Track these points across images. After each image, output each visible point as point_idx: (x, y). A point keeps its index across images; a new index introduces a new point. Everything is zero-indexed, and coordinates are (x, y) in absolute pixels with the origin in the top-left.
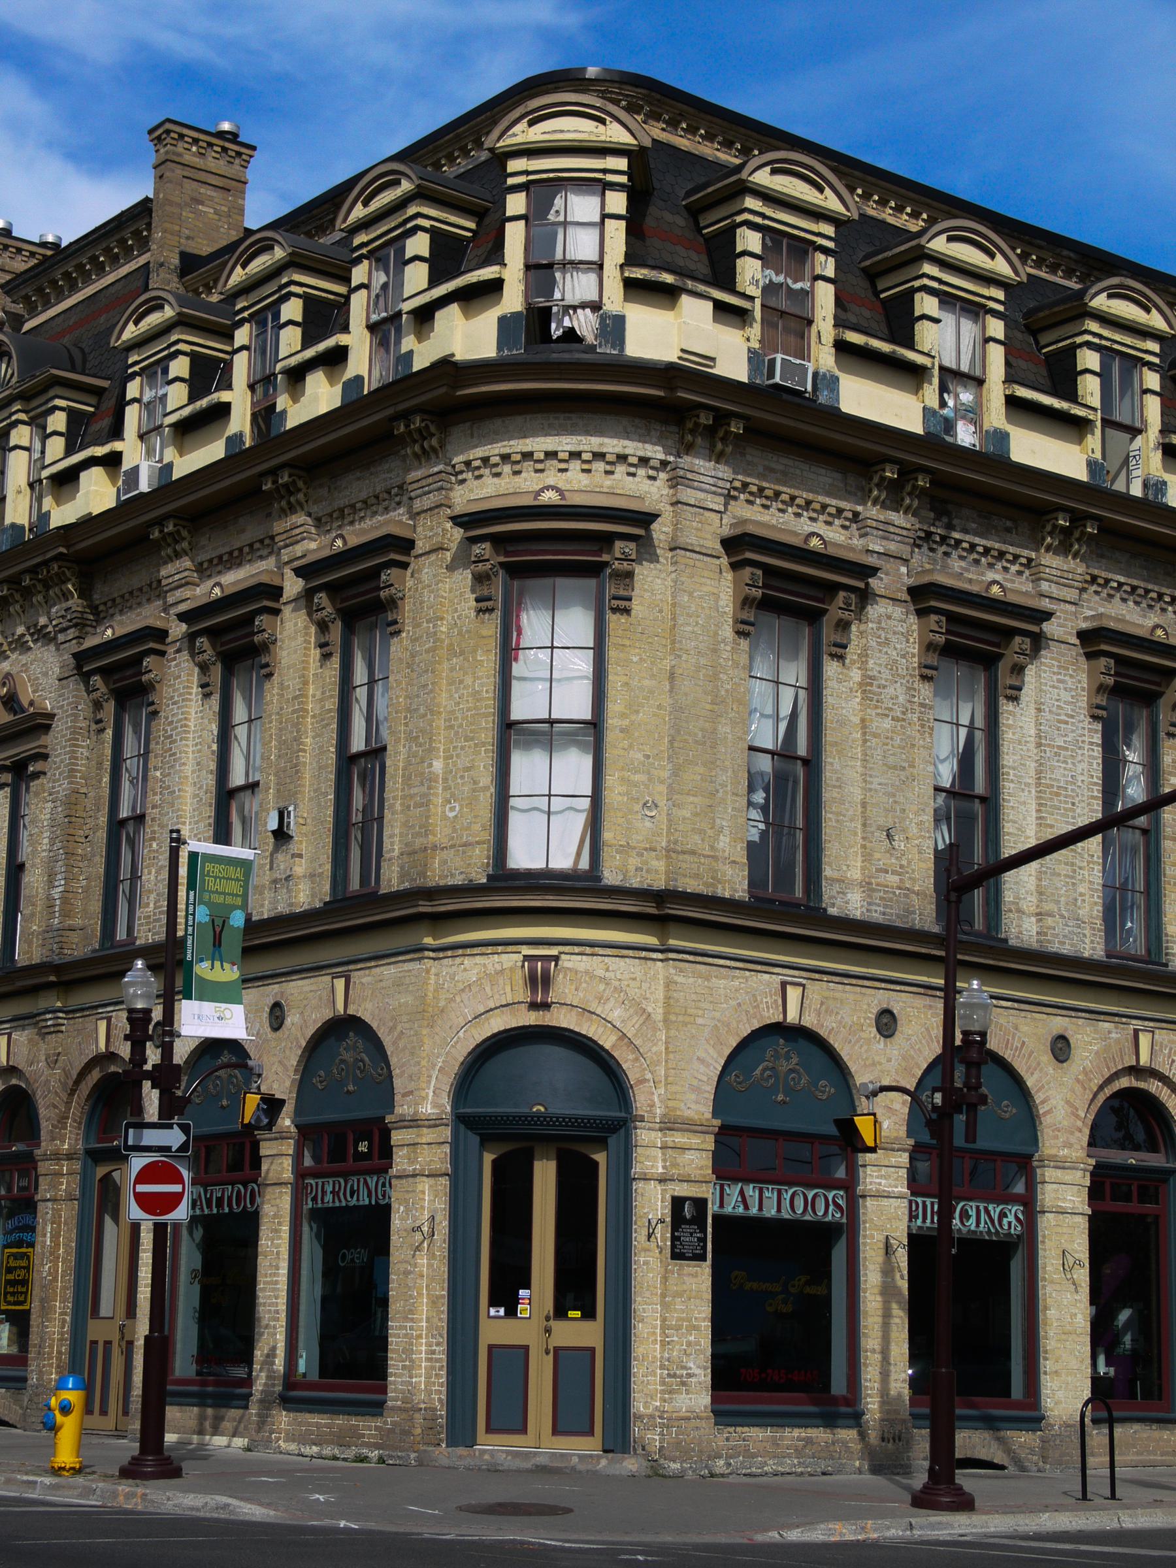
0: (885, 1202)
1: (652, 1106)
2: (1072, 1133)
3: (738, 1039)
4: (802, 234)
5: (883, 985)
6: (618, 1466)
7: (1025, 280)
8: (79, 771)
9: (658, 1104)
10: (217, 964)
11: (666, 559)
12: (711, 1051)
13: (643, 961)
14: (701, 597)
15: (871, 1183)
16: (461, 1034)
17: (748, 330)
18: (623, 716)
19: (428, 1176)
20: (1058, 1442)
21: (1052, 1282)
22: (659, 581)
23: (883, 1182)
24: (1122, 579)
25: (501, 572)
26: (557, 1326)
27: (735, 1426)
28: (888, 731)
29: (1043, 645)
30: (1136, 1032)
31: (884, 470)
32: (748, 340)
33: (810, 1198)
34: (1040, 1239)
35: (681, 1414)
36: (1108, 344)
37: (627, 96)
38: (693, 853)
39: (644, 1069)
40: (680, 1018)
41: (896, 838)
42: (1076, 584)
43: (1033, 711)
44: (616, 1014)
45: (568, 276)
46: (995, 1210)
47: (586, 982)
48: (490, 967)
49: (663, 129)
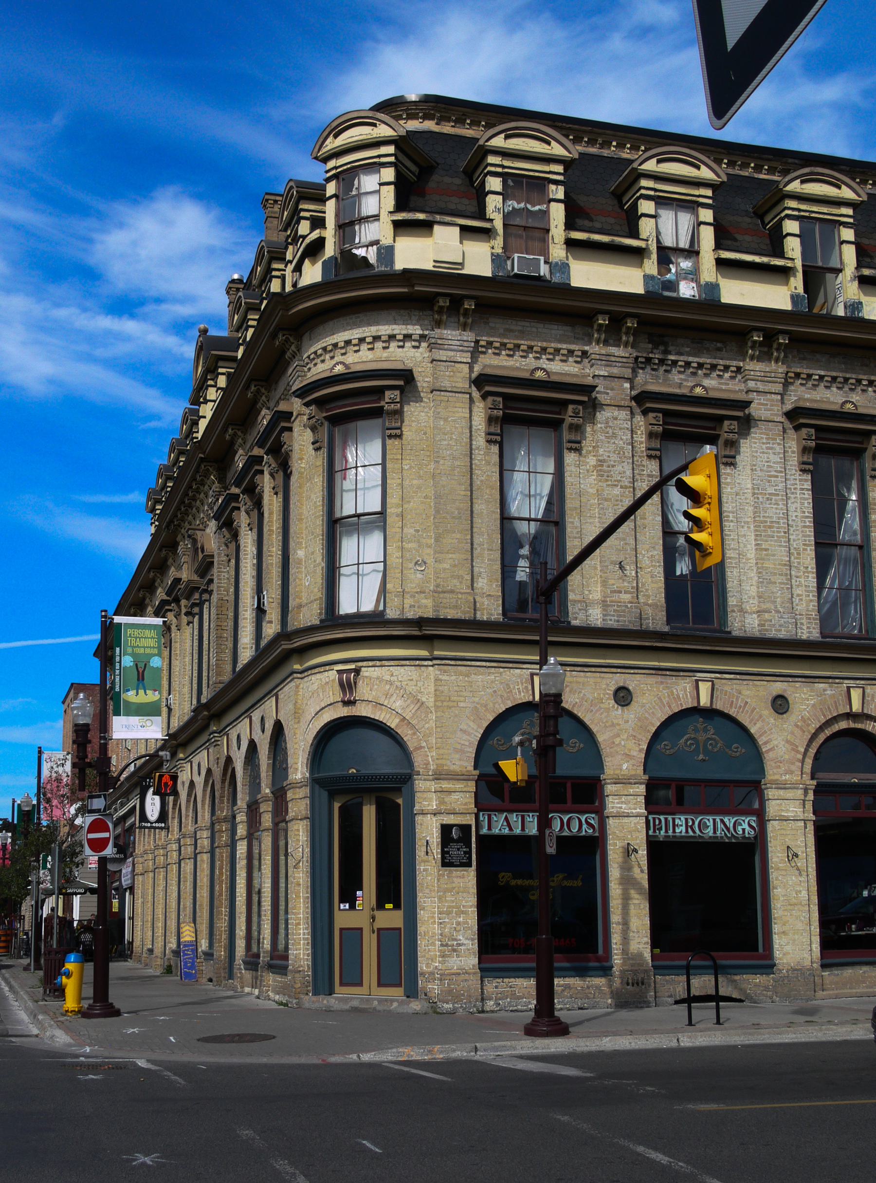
0: (626, 820)
1: (428, 764)
2: (793, 764)
3: (495, 715)
4: (537, 174)
5: (619, 670)
6: (406, 1007)
7: (725, 179)
8: (222, 587)
9: (431, 763)
10: (141, 692)
11: (429, 399)
12: (471, 724)
13: (418, 668)
14: (454, 421)
15: (613, 808)
16: (310, 726)
17: (492, 242)
18: (397, 506)
19: (301, 820)
20: (786, 982)
21: (778, 869)
22: (423, 414)
23: (624, 806)
24: (822, 373)
25: (326, 424)
26: (379, 914)
27: (503, 978)
28: (617, 496)
29: (752, 425)
30: (849, 688)
31: (778, 339)
32: (493, 248)
33: (565, 821)
34: (769, 839)
35: (452, 971)
36: (807, 214)
37: (422, 109)
38: (452, 592)
39: (421, 740)
40: (445, 704)
41: (628, 568)
42: (779, 380)
43: (749, 472)
44: (398, 704)
45: (363, 226)
46: (730, 821)
47: (376, 684)
48: (323, 680)
49: (452, 126)
